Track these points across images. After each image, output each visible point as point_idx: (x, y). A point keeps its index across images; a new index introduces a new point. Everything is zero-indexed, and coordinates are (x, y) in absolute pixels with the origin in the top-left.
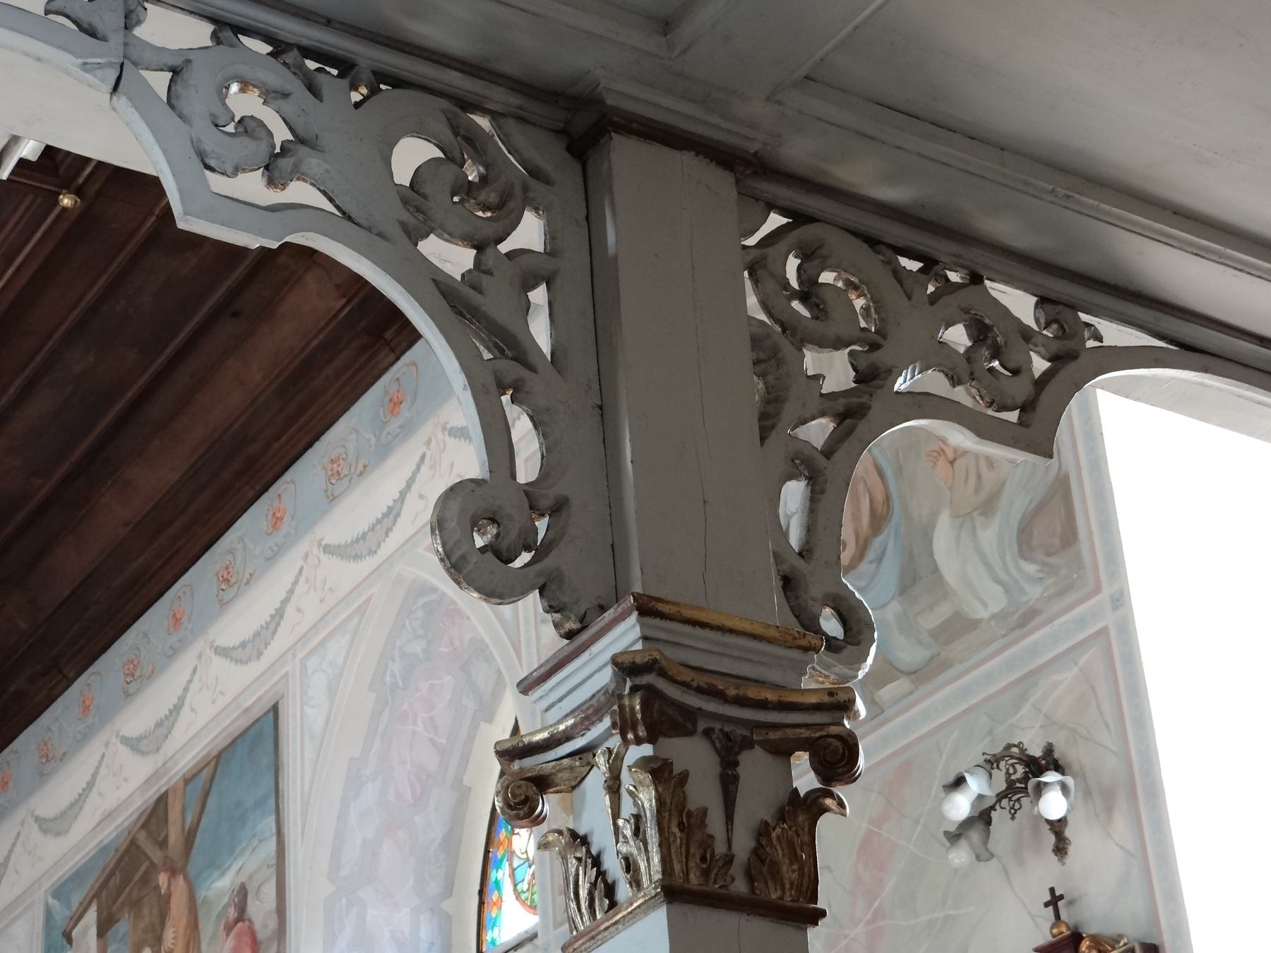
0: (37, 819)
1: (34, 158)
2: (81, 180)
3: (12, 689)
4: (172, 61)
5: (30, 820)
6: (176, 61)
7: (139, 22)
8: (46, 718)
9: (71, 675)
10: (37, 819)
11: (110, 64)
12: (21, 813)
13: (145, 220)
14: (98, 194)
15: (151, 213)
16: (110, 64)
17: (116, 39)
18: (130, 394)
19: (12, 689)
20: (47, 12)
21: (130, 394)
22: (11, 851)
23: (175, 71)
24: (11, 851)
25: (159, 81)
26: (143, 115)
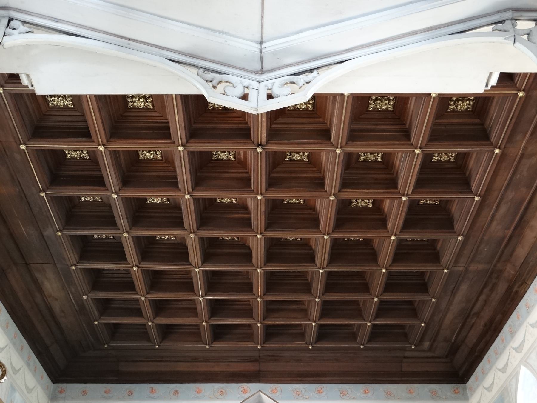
0: (530, 325)
1: (495, 84)
2: (499, 145)
3: (514, 290)
4: (527, 32)
5: (528, 325)
6: (528, 32)
7: (516, 26)
8: (525, 297)
9: (529, 284)
10: (530, 325)
11: (511, 36)
12: (525, 324)
13: (519, 151)
14: (505, 147)
15: (520, 149)
16: (511, 36)
17: (512, 30)
18: (526, 201)
19: (514, 290)
20: (493, 31)
21: (526, 201)
22: (525, 335)
23: (528, 34)
24: (525, 335)
25: (526, 37)
26: (523, 44)
